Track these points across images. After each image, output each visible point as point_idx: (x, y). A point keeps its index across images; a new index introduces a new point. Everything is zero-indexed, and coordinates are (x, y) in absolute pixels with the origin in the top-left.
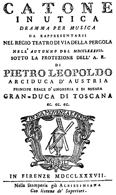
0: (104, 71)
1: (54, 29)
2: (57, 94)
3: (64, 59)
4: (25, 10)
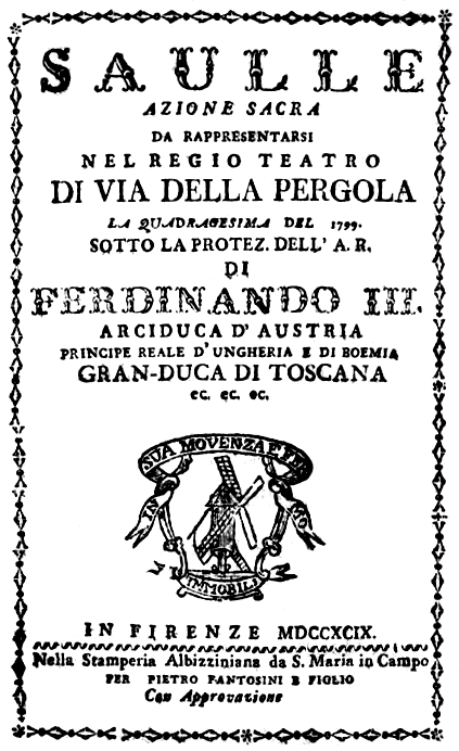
0: (309, 295)
2: (228, 365)
4: (108, 77)
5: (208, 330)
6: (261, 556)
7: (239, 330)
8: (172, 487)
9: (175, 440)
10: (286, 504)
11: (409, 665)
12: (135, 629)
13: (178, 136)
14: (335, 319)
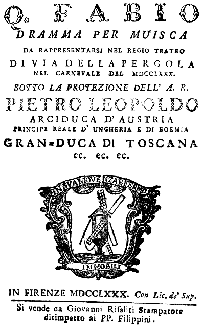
3: (145, 141)
5: (90, 119)
7: (109, 119)
11: (63, 320)
13: (36, 50)
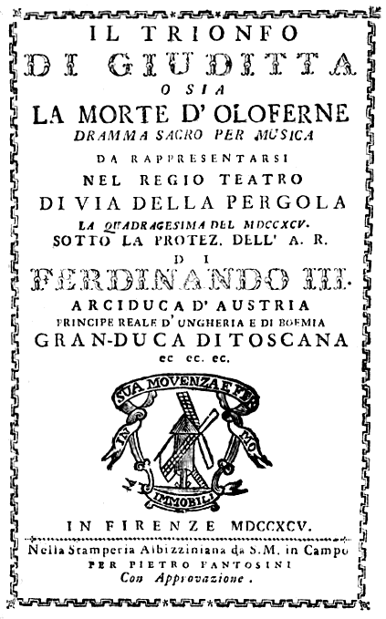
1: (91, 567)
2: (189, 335)
6: (217, 476)
8: (140, 418)
9: (142, 379)
10: (239, 431)
12: (109, 524)
14: (284, 296)
